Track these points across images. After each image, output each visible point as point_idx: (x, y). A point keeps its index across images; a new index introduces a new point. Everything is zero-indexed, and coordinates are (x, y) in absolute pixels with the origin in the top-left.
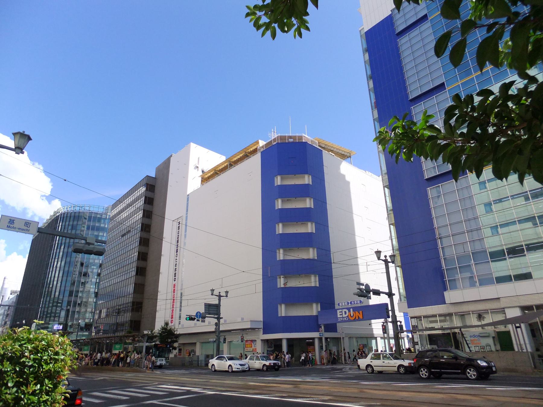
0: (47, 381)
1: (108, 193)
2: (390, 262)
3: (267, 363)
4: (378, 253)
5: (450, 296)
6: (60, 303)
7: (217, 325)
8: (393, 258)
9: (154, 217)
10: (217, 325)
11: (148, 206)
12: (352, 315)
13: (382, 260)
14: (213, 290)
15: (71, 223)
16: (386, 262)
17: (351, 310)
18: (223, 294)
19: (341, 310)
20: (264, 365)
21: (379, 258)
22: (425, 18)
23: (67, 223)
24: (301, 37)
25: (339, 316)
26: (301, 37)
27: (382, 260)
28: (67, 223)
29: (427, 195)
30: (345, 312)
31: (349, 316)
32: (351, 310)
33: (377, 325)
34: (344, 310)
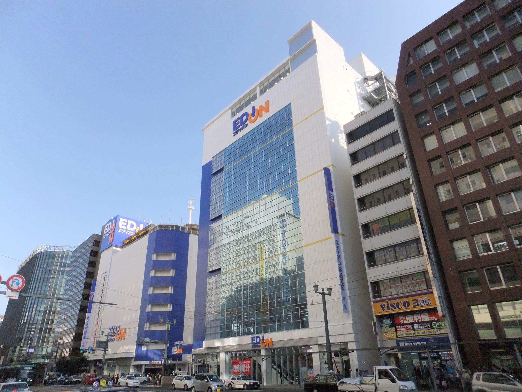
1: (69, 238)
2: (327, 294)
3: (248, 383)
5: (205, 344)
6: (33, 331)
8: (316, 288)
9: (162, 224)
11: (91, 268)
15: (46, 261)
16: (323, 294)
18: (326, 292)
19: (126, 220)
20: (245, 385)
21: (316, 292)
22: (221, 170)
23: (43, 261)
24: (290, 104)
26: (290, 104)
28: (43, 261)
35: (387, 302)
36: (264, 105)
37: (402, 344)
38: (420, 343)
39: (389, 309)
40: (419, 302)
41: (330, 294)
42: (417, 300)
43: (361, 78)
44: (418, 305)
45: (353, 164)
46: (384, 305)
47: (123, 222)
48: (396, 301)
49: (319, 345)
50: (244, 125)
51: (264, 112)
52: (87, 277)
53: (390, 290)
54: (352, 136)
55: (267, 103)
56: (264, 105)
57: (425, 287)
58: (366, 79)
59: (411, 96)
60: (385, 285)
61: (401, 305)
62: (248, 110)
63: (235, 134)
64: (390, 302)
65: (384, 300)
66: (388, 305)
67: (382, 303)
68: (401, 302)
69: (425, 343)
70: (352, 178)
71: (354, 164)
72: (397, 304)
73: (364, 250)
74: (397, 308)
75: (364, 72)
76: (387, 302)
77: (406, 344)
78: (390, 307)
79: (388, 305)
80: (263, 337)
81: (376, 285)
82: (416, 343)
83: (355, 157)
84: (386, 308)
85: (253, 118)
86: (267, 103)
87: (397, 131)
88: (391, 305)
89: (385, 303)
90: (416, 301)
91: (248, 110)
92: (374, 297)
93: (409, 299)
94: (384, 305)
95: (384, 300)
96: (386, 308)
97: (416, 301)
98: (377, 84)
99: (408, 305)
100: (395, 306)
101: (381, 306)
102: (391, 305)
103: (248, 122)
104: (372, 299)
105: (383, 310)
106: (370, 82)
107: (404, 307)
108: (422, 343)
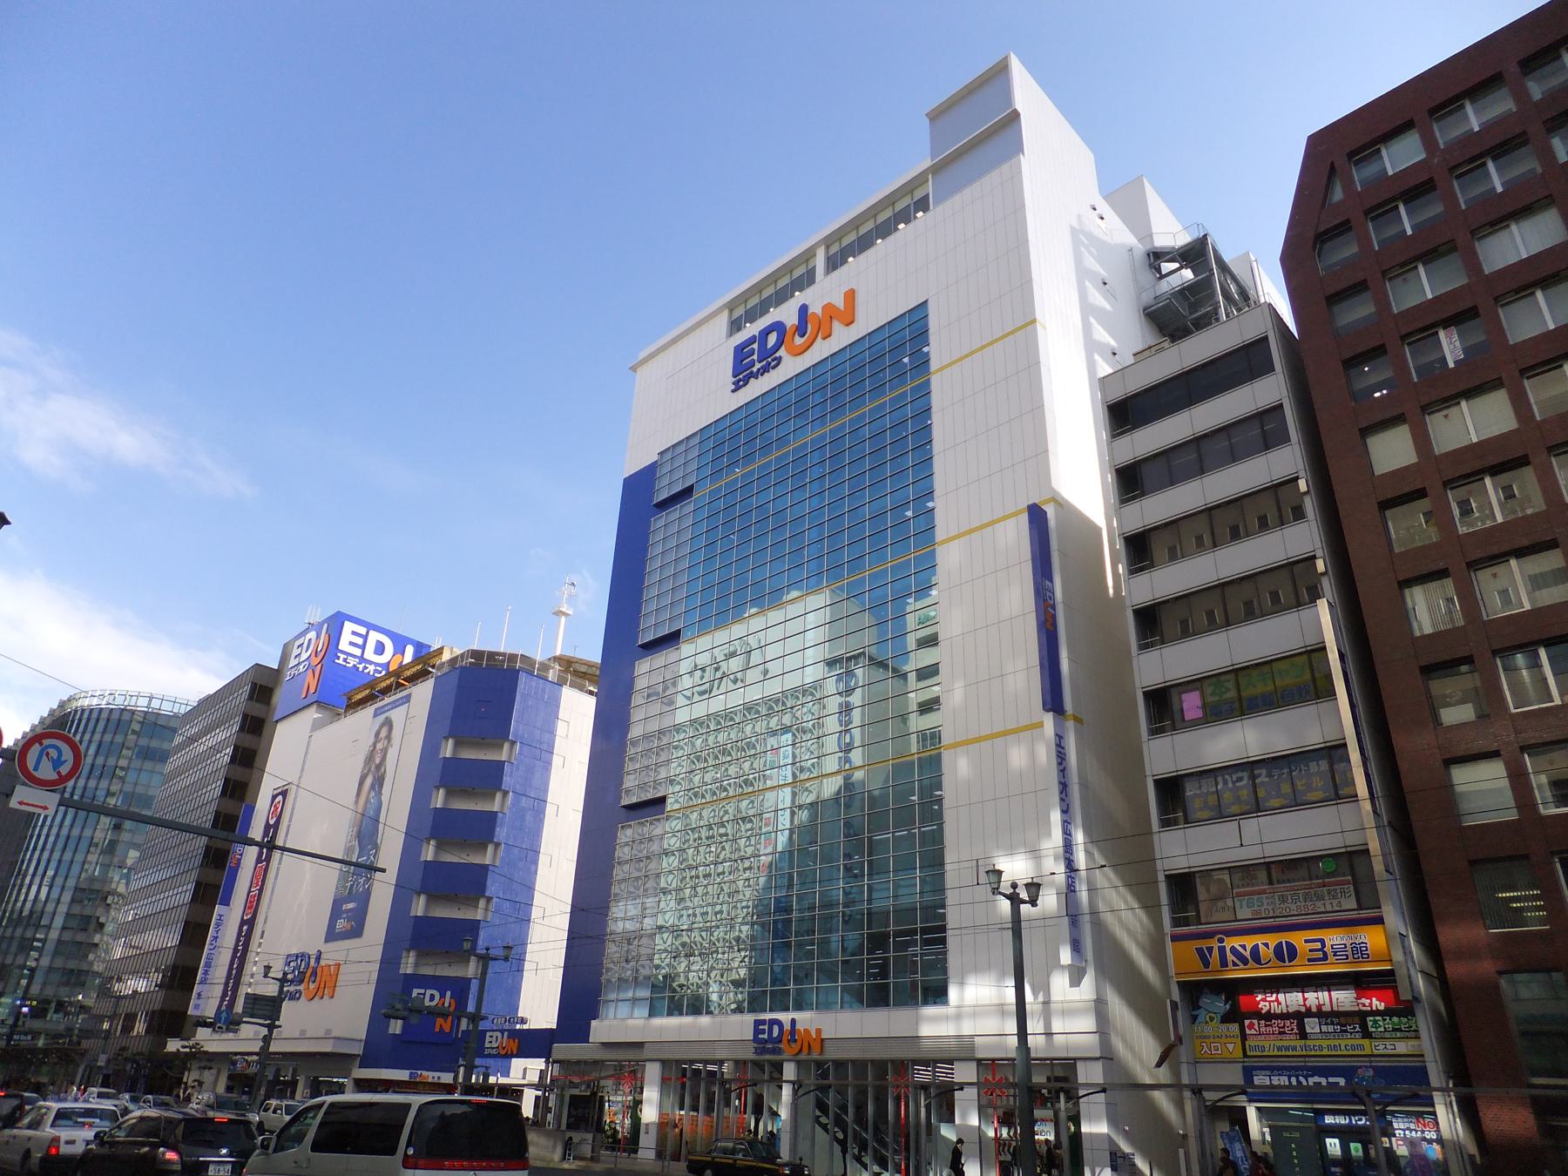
7: (267, 1040)
10: (267, 1040)
16: (1014, 899)
19: (363, 630)
29: (615, 837)
33: (1257, 1081)
34: (429, 992)
35: (1221, 941)
36: (839, 303)
38: (1324, 1081)
41: (1033, 903)
42: (1322, 941)
44: (1325, 957)
49: (979, 1061)
50: (770, 361)
53: (1229, 902)
56: (839, 303)
62: (787, 313)
63: (737, 387)
67: (1204, 944)
68: (1266, 945)
69: (1342, 1081)
71: (1128, 500)
79: (1222, 950)
80: (793, 1021)
82: (1312, 1081)
83: (1140, 549)
85: (799, 341)
86: (850, 296)
91: (787, 313)
92: (1176, 922)
95: (1209, 935)
98: (1188, 274)
101: (1200, 951)
102: (1233, 949)
103: (782, 352)
106: (1167, 267)
108: (1331, 1080)
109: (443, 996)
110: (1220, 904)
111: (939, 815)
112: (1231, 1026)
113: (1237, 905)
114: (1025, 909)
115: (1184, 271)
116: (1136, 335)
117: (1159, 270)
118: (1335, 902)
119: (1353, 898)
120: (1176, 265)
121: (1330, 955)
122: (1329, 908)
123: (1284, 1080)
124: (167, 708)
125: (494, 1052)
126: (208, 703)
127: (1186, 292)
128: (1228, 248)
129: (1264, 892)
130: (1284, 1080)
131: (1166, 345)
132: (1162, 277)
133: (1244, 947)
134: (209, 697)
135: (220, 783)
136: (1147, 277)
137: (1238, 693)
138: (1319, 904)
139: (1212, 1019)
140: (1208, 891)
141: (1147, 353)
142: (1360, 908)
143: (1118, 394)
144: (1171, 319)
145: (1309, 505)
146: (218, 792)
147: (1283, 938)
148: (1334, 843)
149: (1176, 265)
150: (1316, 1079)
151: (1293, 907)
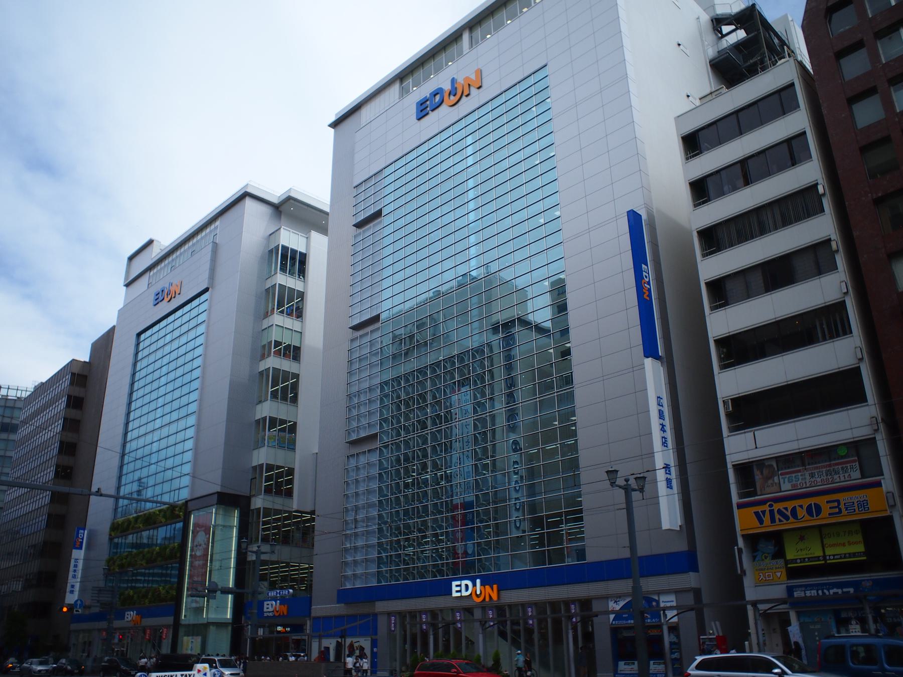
0: (741, 34)
2: (635, 490)
4: (612, 473)
12: (478, 593)
13: (620, 487)
14: (612, 473)
16: (627, 489)
17: (478, 581)
19: (458, 583)
21: (613, 484)
25: (265, 610)
27: (620, 487)
30: (467, 586)
31: (474, 596)
32: (478, 581)
33: (796, 594)
34: (464, 582)
35: (771, 506)
37: (797, 594)
38: (840, 591)
39: (773, 520)
40: (842, 506)
41: (641, 490)
42: (838, 501)
43: (705, 18)
44: (840, 511)
45: (696, 206)
46: (764, 512)
47: (827, 502)
48: (790, 505)
51: (474, 91)
52: (61, 451)
53: (776, 479)
54: (692, 144)
55: (479, 73)
57: (856, 474)
58: (718, 22)
59: (841, 54)
60: (765, 472)
61: (801, 513)
64: (776, 507)
65: (763, 502)
66: (772, 512)
67: (759, 509)
68: (801, 506)
69: (852, 590)
70: (695, 235)
71: (700, 204)
72: (794, 511)
73: (719, 396)
74: (791, 519)
75: (713, 6)
76: (771, 506)
77: (808, 593)
78: (777, 516)
79: (772, 512)
81: (745, 470)
82: (832, 592)
83: (701, 190)
84: (767, 519)
85: (453, 99)
87: (804, 133)
88: (779, 511)
89: (766, 507)
90: (836, 504)
92: (741, 496)
93: (821, 500)
94: (764, 512)
95: (763, 502)
96: (767, 519)
97: (836, 504)
98: (741, 34)
99: (809, 508)
100: (789, 514)
101: (757, 513)
102: (779, 511)
104: (735, 499)
105: (761, 521)
106: (726, 29)
107: (807, 517)
108: (845, 590)
109: (474, 585)
110: (770, 482)
111: (574, 434)
112: (778, 561)
113: (782, 481)
114: (636, 495)
115: (739, 31)
116: (702, 80)
117: (721, 32)
118: (846, 475)
119: (858, 472)
120: (733, 27)
121: (843, 510)
122: (842, 479)
123: (814, 593)
124: (12, 394)
125: (271, 614)
126: (41, 388)
127: (739, 46)
128: (771, 14)
129: (799, 471)
130: (814, 593)
131: (725, 90)
132: (723, 36)
133: (786, 509)
134: (42, 384)
135: (57, 445)
136: (710, 37)
137: (777, 273)
138: (836, 477)
139: (766, 558)
140: (762, 473)
141: (709, 98)
142: (863, 477)
143: (691, 126)
144: (728, 70)
145: (827, 203)
146: (56, 451)
147: (812, 501)
148: (846, 436)
149: (733, 27)
150: (835, 590)
151: (819, 480)
